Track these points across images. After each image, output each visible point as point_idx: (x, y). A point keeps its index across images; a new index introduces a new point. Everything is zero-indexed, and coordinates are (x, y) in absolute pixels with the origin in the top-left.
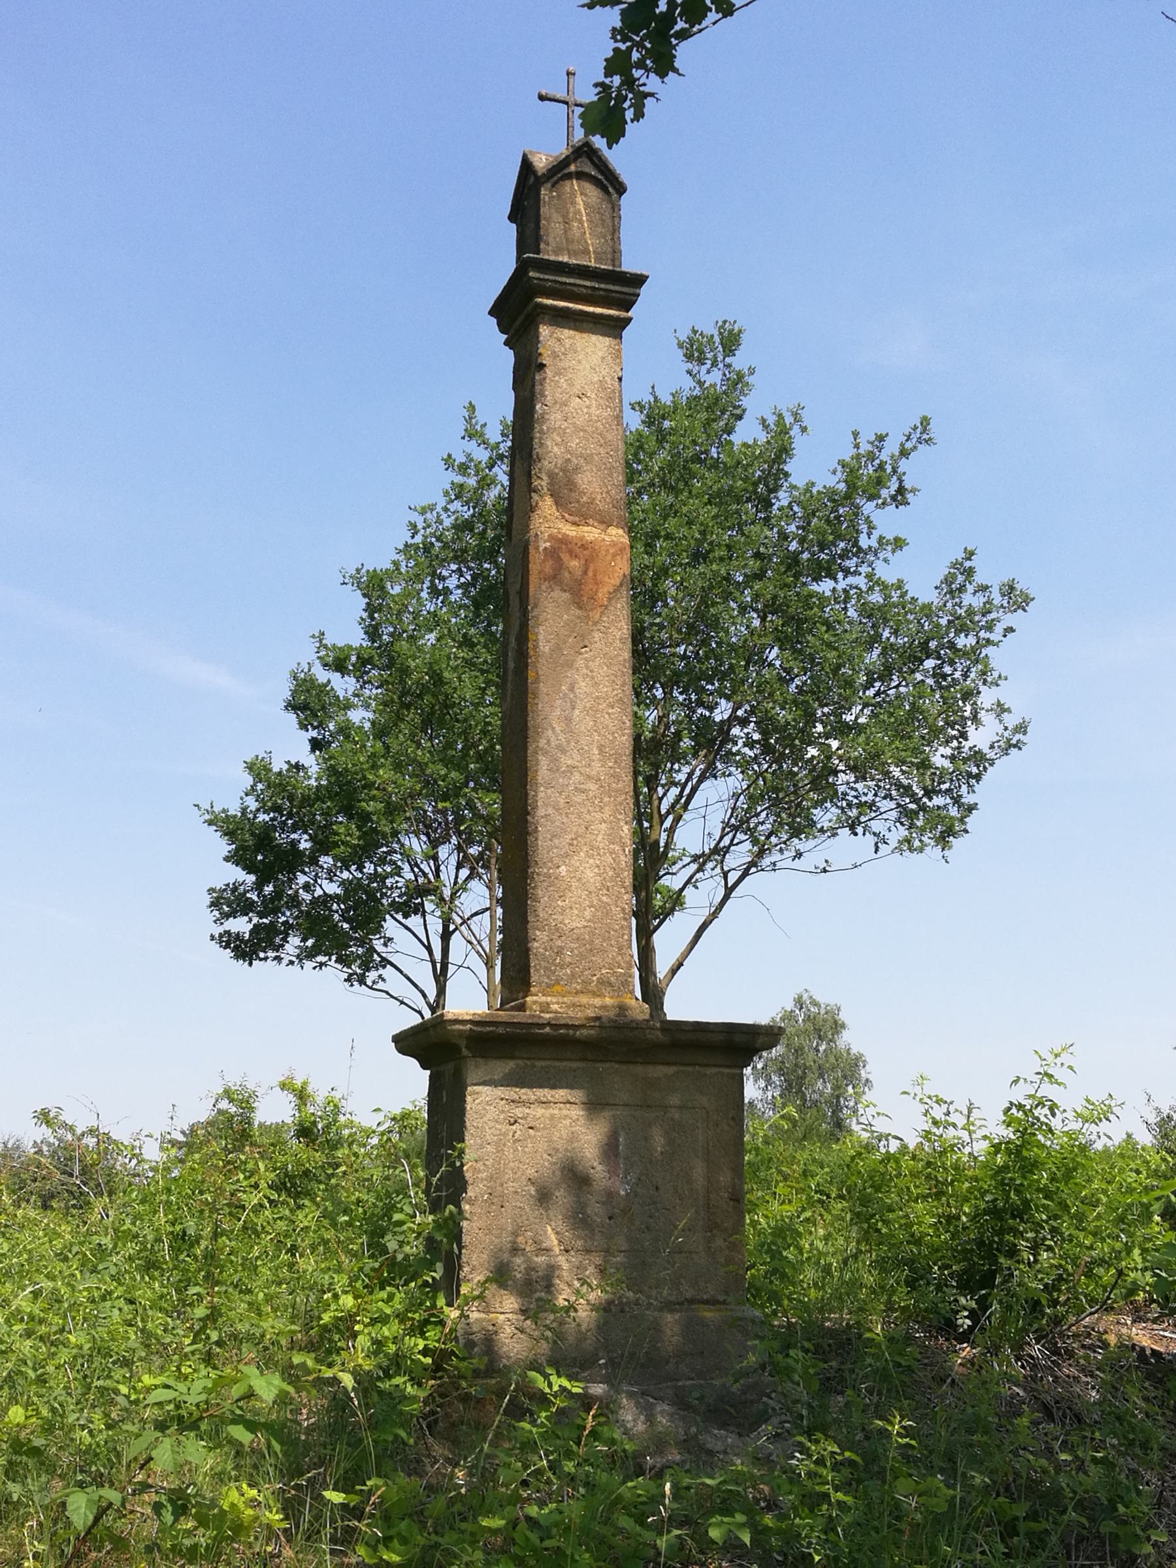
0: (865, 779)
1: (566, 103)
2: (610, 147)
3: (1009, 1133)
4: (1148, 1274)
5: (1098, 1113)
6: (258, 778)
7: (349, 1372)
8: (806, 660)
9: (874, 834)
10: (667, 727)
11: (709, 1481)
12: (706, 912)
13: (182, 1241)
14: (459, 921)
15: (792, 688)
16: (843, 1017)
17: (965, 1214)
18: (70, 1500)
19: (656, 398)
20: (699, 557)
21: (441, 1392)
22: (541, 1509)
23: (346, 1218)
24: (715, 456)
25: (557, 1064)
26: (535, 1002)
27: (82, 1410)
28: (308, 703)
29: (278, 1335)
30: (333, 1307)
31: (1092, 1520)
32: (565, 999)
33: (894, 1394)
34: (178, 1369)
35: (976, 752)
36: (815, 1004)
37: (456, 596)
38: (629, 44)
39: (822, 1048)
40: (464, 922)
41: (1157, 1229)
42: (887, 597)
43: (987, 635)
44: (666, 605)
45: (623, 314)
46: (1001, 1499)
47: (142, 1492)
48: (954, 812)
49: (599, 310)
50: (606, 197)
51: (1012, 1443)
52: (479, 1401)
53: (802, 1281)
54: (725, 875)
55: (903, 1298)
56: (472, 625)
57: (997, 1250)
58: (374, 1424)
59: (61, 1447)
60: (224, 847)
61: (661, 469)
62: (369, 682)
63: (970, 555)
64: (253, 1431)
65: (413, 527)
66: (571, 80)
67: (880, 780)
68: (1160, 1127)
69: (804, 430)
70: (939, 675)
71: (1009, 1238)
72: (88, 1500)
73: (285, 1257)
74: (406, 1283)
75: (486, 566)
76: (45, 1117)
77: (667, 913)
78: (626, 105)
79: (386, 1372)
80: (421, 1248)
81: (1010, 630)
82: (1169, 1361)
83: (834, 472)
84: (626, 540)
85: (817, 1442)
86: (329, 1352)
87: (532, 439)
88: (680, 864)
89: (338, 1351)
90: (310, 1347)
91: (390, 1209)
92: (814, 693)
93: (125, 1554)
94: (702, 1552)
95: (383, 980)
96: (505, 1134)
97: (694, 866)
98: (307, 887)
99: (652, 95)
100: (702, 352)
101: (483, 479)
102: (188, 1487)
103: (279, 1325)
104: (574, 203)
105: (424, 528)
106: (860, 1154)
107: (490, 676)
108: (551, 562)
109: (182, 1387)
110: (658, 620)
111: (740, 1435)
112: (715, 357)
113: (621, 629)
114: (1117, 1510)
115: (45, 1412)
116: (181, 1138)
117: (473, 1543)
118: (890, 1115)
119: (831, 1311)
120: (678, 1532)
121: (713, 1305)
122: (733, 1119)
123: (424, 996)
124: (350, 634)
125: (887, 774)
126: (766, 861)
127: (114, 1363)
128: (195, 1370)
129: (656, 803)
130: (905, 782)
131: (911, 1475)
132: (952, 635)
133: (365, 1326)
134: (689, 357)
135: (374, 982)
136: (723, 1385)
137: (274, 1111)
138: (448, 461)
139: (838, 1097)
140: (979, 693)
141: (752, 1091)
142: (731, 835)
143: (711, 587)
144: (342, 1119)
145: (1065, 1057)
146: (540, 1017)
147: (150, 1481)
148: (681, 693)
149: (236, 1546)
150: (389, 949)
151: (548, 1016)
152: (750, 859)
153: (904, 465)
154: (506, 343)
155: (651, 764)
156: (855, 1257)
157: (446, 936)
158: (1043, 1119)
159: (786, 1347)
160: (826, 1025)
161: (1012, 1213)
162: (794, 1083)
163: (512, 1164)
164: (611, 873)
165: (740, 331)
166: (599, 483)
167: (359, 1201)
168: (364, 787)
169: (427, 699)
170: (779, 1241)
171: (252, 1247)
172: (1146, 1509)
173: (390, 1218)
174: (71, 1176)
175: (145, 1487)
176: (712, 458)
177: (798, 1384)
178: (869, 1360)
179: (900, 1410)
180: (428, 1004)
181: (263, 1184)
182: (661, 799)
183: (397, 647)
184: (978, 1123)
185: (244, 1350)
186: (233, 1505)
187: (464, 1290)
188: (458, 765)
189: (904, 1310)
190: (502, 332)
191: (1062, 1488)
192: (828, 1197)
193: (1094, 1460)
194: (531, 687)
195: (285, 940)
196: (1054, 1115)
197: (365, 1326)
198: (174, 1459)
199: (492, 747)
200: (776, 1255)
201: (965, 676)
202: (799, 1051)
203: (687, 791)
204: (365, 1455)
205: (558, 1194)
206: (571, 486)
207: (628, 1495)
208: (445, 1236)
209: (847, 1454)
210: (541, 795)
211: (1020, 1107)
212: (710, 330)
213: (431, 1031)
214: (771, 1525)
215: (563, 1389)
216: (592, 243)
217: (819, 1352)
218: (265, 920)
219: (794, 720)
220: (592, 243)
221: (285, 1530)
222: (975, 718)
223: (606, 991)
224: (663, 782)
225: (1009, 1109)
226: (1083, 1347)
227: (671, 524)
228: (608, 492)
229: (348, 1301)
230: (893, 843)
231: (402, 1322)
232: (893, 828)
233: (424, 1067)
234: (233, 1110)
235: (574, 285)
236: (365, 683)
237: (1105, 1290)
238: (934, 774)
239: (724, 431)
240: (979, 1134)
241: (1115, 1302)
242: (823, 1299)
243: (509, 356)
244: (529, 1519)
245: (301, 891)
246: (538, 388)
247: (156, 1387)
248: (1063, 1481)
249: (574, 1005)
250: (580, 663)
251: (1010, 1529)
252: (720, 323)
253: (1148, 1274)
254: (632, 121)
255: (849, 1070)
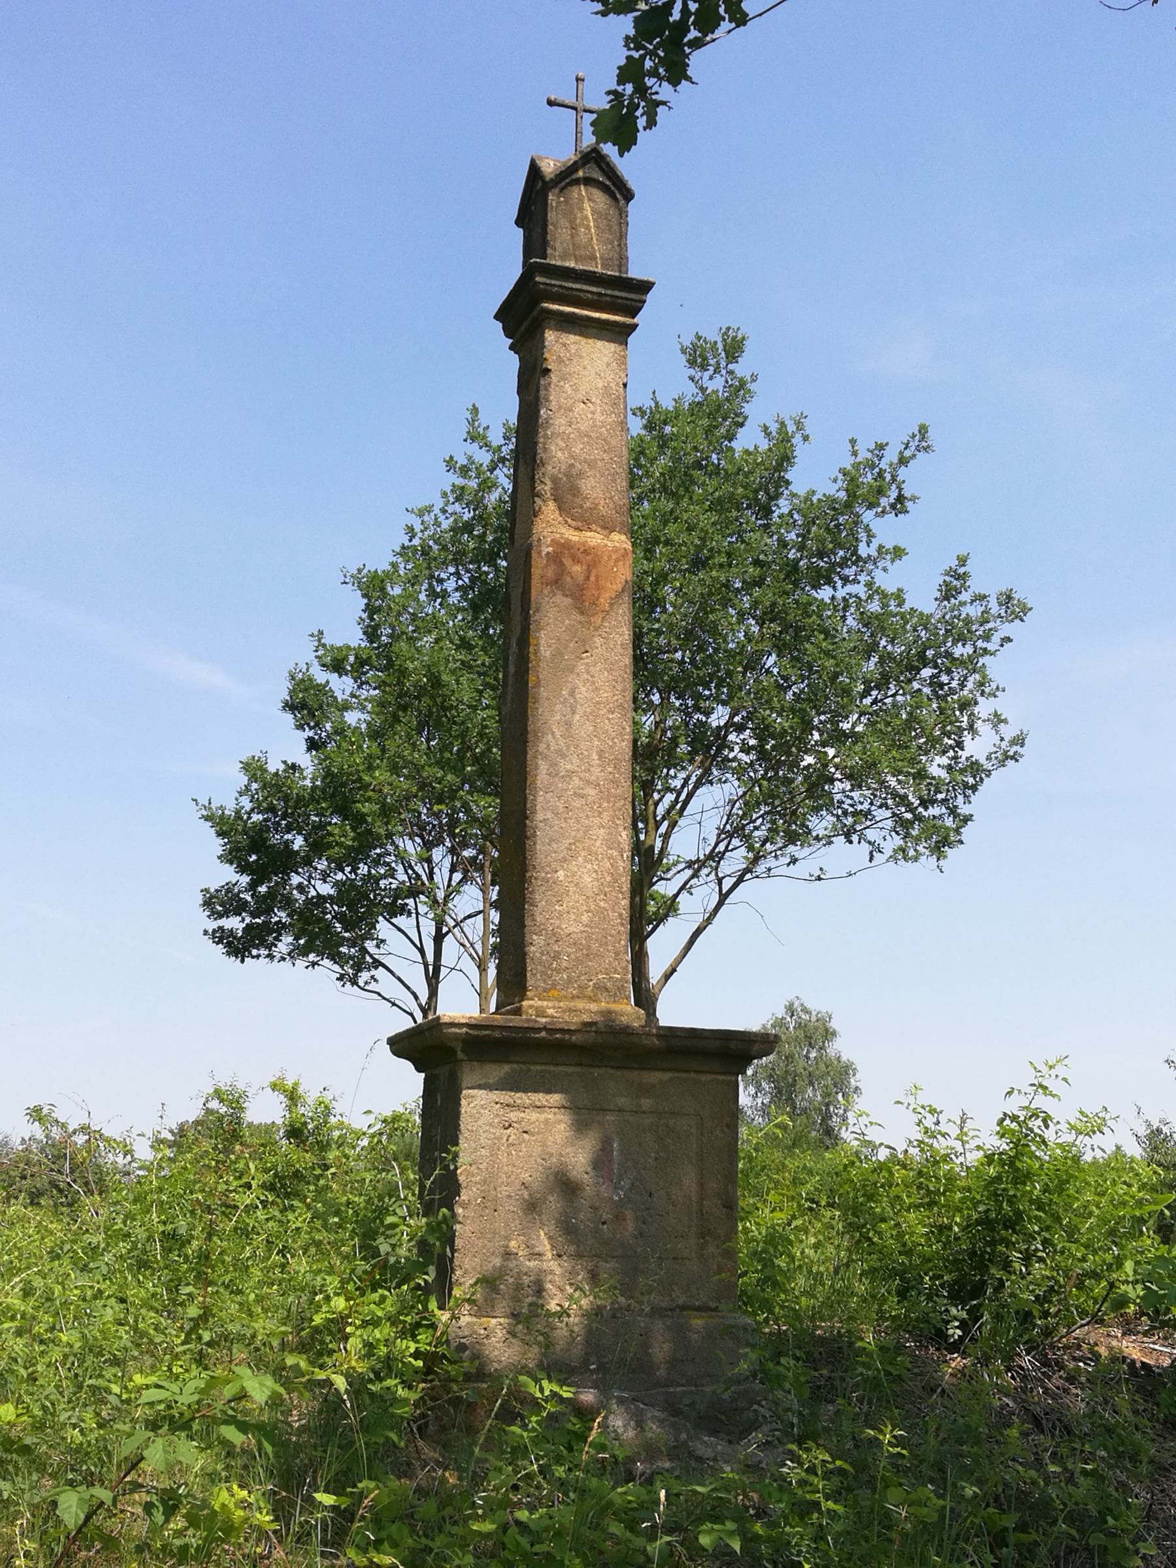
0: (860, 787)
1: (575, 109)
2: (621, 155)
3: (1003, 1145)
4: (1139, 1287)
5: (1093, 1126)
6: (253, 778)
7: (342, 1374)
8: (806, 669)
9: (869, 843)
10: (664, 732)
11: (699, 1489)
12: (699, 919)
13: (173, 1241)
14: (452, 923)
15: (789, 696)
16: (834, 1025)
17: (956, 1224)
18: (61, 1499)
19: (657, 403)
20: (699, 564)
21: (430, 1396)
22: (531, 1514)
23: (336, 1220)
24: (716, 462)
25: (552, 1068)
26: (531, 1007)
27: (74, 1409)
28: (306, 703)
29: (268, 1335)
30: (324, 1309)
31: (1081, 1532)
32: (562, 1004)
33: (884, 1404)
34: (170, 1369)
35: (972, 763)
36: (806, 1011)
37: (455, 598)
38: (642, 52)
39: (813, 1055)
40: (457, 924)
41: (1149, 1242)
42: (884, 606)
43: (985, 645)
44: (664, 610)
45: (628, 320)
46: (991, 1510)
47: (132, 1491)
48: (949, 822)
49: (604, 316)
50: (613, 203)
51: (1002, 1454)
52: (470, 1405)
53: (793, 1289)
54: (720, 882)
55: (894, 1307)
56: (470, 628)
57: (989, 1260)
58: (366, 1427)
59: (51, 1446)
60: (217, 845)
61: (662, 474)
62: (367, 683)
63: (963, 561)
64: (245, 1433)
65: (411, 531)
66: (580, 87)
67: (876, 790)
68: (1150, 1140)
69: (806, 438)
70: (935, 683)
71: (1001, 1248)
72: (80, 1499)
73: (276, 1258)
74: (398, 1286)
75: (485, 569)
76: (37, 1114)
77: (660, 919)
78: (638, 113)
79: (377, 1374)
80: (415, 1251)
81: (1008, 640)
82: (1159, 1374)
83: (835, 481)
84: (629, 546)
85: (808, 1450)
86: (320, 1354)
87: (536, 443)
88: (674, 870)
89: (331, 1353)
90: (302, 1348)
91: (382, 1212)
92: (810, 700)
93: (113, 1552)
94: (691, 1559)
95: (376, 980)
96: (499, 1138)
97: (689, 872)
98: (301, 888)
99: (664, 103)
100: (705, 359)
101: (484, 481)
102: (179, 1487)
103: (271, 1325)
104: (581, 209)
105: (422, 531)
106: (853, 1163)
107: (487, 679)
108: (553, 567)
109: (175, 1387)
110: (656, 626)
111: (730, 1442)
112: (718, 363)
113: (624, 635)
114: (1106, 1522)
115: (38, 1412)
116: (170, 1137)
117: (464, 1547)
118: (881, 1121)
119: (822, 1319)
120: (669, 1539)
121: (705, 1311)
122: (727, 1125)
123: (416, 998)
124: (349, 634)
125: (882, 782)
126: (761, 868)
127: (104, 1362)
128: (187, 1371)
129: (652, 808)
130: (902, 792)
131: (901, 1485)
132: (949, 644)
133: (357, 1328)
134: (692, 363)
135: (366, 983)
136: (714, 1392)
137: (264, 1110)
138: (450, 463)
139: (827, 1105)
140: (976, 703)
141: (745, 1099)
142: (726, 842)
143: (710, 594)
144: (333, 1120)
145: (1059, 1070)
146: (536, 1021)
147: (140, 1480)
148: (677, 699)
149: (227, 1547)
150: (382, 951)
151: (544, 1020)
152: (745, 866)
153: (903, 473)
154: (511, 348)
155: (648, 770)
156: (847, 1265)
157: (439, 939)
158: (1037, 1131)
159: (777, 1356)
160: (817, 1033)
161: (1004, 1224)
162: (784, 1091)
163: (505, 1168)
164: (608, 879)
165: (744, 338)
166: (602, 488)
167: (348, 1203)
168: (359, 789)
169: (426, 700)
170: (771, 1250)
171: (243, 1248)
172: (1134, 1522)
173: (382, 1222)
174: (59, 1174)
175: (136, 1487)
176: (713, 464)
177: (789, 1392)
178: (860, 1370)
179: (891, 1419)
180: (420, 1005)
181: (254, 1184)
182: (656, 804)
183: (395, 649)
184: (971, 1134)
185: (234, 1351)
186: (223, 1505)
187: (457, 1292)
188: (454, 768)
189: (894, 1319)
190: (507, 336)
191: (1052, 1499)
192: (817, 1203)
193: (1084, 1472)
194: (531, 691)
195: (277, 939)
196: (1047, 1127)
197: (357, 1328)
198: (167, 1459)
199: (489, 750)
200: (768, 1263)
201: (962, 685)
202: (789, 1058)
203: (683, 797)
204: (356, 1456)
205: (551, 1199)
206: (575, 491)
207: (618, 1501)
208: (438, 1239)
209: (838, 1463)
210: (540, 799)
211: (1014, 1118)
212: (713, 336)
213: (427, 1034)
214: (761, 1532)
215: (554, 1394)
216: (599, 249)
217: (811, 1361)
218: (258, 920)
219: (791, 728)
220: (599, 249)
221: (275, 1532)
222: (971, 728)
223: (603, 996)
224: (659, 787)
225: (1003, 1120)
226: (1075, 1359)
227: (671, 529)
228: (611, 498)
229: (340, 1303)
230: (888, 852)
231: (393, 1324)
232: (888, 837)
233: (419, 1070)
234: (223, 1110)
235: (580, 290)
236: (362, 683)
237: (1096, 1302)
238: (931, 784)
239: (725, 438)
240: (973, 1144)
241: (1105, 1314)
242: (814, 1308)
243: (514, 361)
244: (518, 1523)
245: (295, 892)
246: (542, 393)
247: (148, 1387)
248: (1052, 1492)
249: (570, 1010)
250: (581, 668)
251: (999, 1540)
252: (724, 330)
253: (1139, 1287)
254: (645, 129)
255: (840, 1077)
